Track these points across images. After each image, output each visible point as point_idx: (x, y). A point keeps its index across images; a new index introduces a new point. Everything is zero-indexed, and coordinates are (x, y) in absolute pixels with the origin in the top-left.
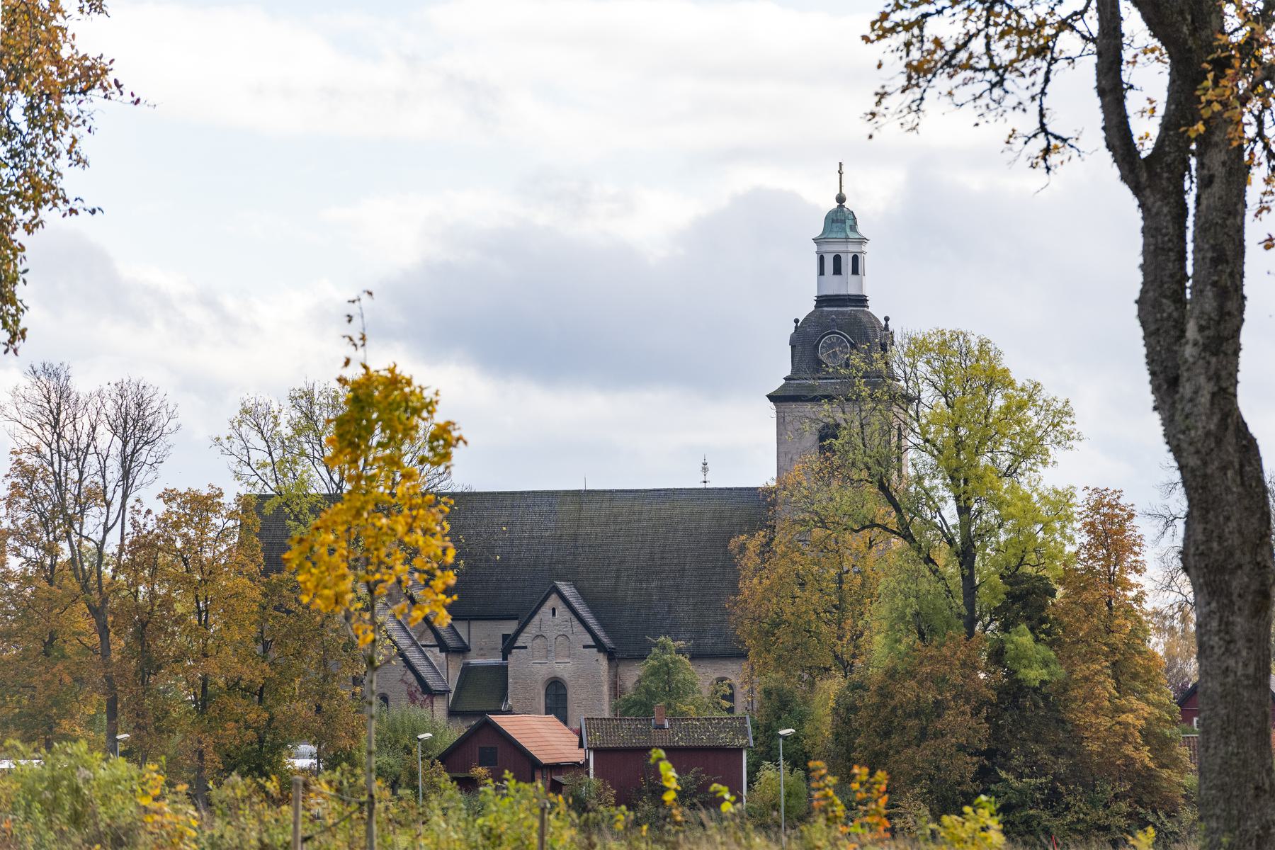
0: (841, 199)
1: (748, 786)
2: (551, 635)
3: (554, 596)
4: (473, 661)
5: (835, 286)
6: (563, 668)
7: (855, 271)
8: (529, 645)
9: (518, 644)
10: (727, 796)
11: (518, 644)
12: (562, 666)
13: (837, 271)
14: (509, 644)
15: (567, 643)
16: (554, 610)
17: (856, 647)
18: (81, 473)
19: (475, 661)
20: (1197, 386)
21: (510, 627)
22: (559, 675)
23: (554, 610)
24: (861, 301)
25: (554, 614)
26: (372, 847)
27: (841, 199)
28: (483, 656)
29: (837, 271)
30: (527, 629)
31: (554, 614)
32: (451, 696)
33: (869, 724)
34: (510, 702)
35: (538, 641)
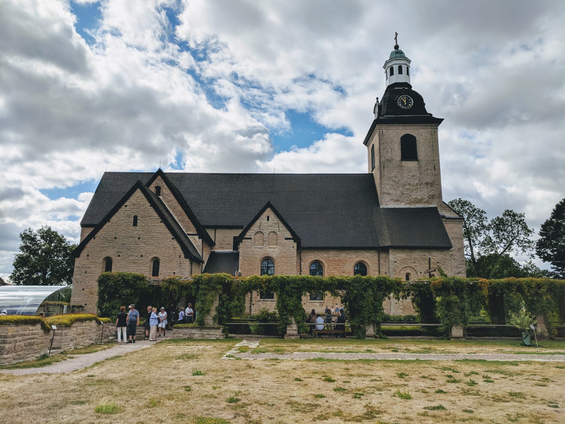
0: (397, 47)
1: (426, 326)
2: (266, 232)
3: (269, 209)
4: (216, 251)
5: (397, 78)
6: (273, 251)
7: (400, 72)
8: (253, 237)
9: (246, 236)
10: (261, 347)
11: (246, 236)
12: (272, 250)
13: (392, 73)
14: (237, 241)
16: (268, 217)
17: (131, 379)
19: (217, 250)
21: (237, 233)
23: (268, 217)
25: (268, 220)
26: (2, 367)
27: (397, 47)
28: (222, 248)
29: (392, 73)
30: (252, 228)
31: (268, 220)
32: (204, 266)
33: (427, 290)
34: (240, 271)
35: (258, 235)
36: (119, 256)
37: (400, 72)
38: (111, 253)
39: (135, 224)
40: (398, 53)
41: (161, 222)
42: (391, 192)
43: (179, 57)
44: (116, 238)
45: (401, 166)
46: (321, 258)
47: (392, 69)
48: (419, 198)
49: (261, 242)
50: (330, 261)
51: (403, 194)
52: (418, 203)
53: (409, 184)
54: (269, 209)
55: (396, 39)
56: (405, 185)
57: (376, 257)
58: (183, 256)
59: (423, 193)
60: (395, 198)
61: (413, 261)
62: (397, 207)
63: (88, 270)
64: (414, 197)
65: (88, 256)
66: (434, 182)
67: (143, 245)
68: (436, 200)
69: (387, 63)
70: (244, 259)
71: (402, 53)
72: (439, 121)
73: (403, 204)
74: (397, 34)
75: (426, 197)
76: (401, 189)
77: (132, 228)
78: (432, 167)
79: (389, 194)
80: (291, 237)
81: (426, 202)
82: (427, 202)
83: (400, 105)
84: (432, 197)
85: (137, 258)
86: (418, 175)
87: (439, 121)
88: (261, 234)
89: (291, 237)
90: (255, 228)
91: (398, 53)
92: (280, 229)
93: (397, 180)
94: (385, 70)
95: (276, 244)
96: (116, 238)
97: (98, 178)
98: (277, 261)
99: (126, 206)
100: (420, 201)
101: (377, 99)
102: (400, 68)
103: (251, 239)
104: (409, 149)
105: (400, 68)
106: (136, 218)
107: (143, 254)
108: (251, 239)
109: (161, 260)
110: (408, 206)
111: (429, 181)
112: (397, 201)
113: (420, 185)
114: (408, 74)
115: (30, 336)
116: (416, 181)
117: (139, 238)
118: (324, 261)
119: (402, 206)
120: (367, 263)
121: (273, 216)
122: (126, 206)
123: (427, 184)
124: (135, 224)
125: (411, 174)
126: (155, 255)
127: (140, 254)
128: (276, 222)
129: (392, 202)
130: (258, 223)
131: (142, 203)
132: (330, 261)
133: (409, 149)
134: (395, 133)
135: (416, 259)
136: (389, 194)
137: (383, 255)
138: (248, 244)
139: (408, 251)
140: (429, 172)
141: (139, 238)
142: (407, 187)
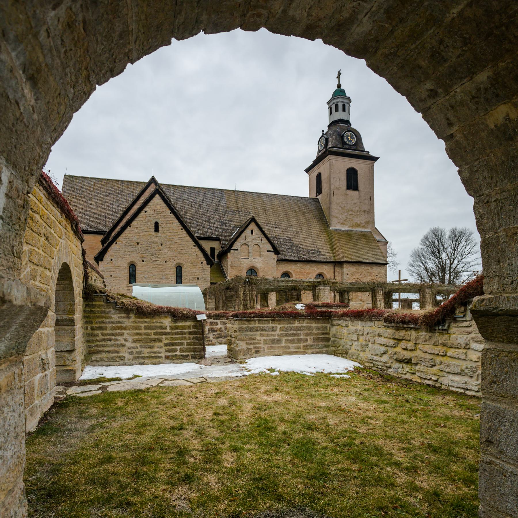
0: (339, 86)
3: (253, 224)
5: (340, 115)
6: (258, 262)
7: (344, 110)
11: (233, 248)
12: (256, 260)
13: (337, 110)
15: (258, 249)
16: (252, 231)
18: (253, 317)
20: (66, 323)
22: (255, 265)
23: (252, 231)
24: (347, 122)
25: (252, 233)
27: (339, 86)
29: (337, 110)
30: (238, 240)
31: (252, 233)
35: (244, 247)
36: (143, 261)
37: (344, 110)
38: (135, 258)
39: (157, 230)
40: (340, 92)
41: (182, 229)
42: (338, 215)
44: (138, 243)
45: (346, 195)
46: (291, 269)
47: (337, 106)
48: (359, 223)
49: (247, 253)
50: (297, 272)
51: (347, 218)
52: (357, 227)
53: (352, 210)
54: (253, 224)
55: (338, 77)
56: (349, 211)
57: (332, 270)
58: (205, 262)
59: (361, 219)
60: (341, 221)
61: (360, 274)
62: (343, 229)
63: (112, 274)
64: (355, 221)
65: (112, 260)
66: (369, 210)
67: (166, 251)
68: (370, 226)
70: (232, 268)
72: (375, 159)
73: (347, 227)
74: (340, 74)
75: (363, 222)
76: (346, 214)
77: (154, 233)
78: (369, 197)
79: (337, 217)
80: (272, 250)
81: (363, 227)
82: (364, 227)
83: (346, 140)
84: (368, 223)
85: (161, 263)
86: (358, 203)
87: (375, 159)
88: (247, 246)
89: (272, 250)
90: (241, 240)
91: (340, 92)
92: (263, 242)
93: (343, 206)
94: (328, 106)
95: (260, 256)
96: (138, 243)
98: (260, 270)
99: (146, 212)
100: (359, 226)
101: (323, 131)
103: (237, 250)
104: (352, 180)
106: (157, 224)
107: (167, 260)
108: (237, 250)
109: (185, 266)
110: (350, 229)
111: (366, 209)
112: (343, 224)
113: (360, 212)
116: (357, 208)
117: (162, 244)
118: (292, 272)
119: (346, 228)
120: (325, 275)
121: (256, 230)
122: (146, 212)
123: (364, 211)
124: (157, 230)
125: (353, 202)
126: (179, 261)
127: (164, 260)
128: (259, 236)
129: (339, 224)
130: (243, 235)
131: (162, 210)
132: (297, 272)
133: (352, 180)
134: (342, 164)
135: (362, 272)
136: (337, 217)
137: (337, 269)
138: (235, 254)
139: (356, 265)
140: (366, 201)
141: (162, 244)
142: (350, 213)
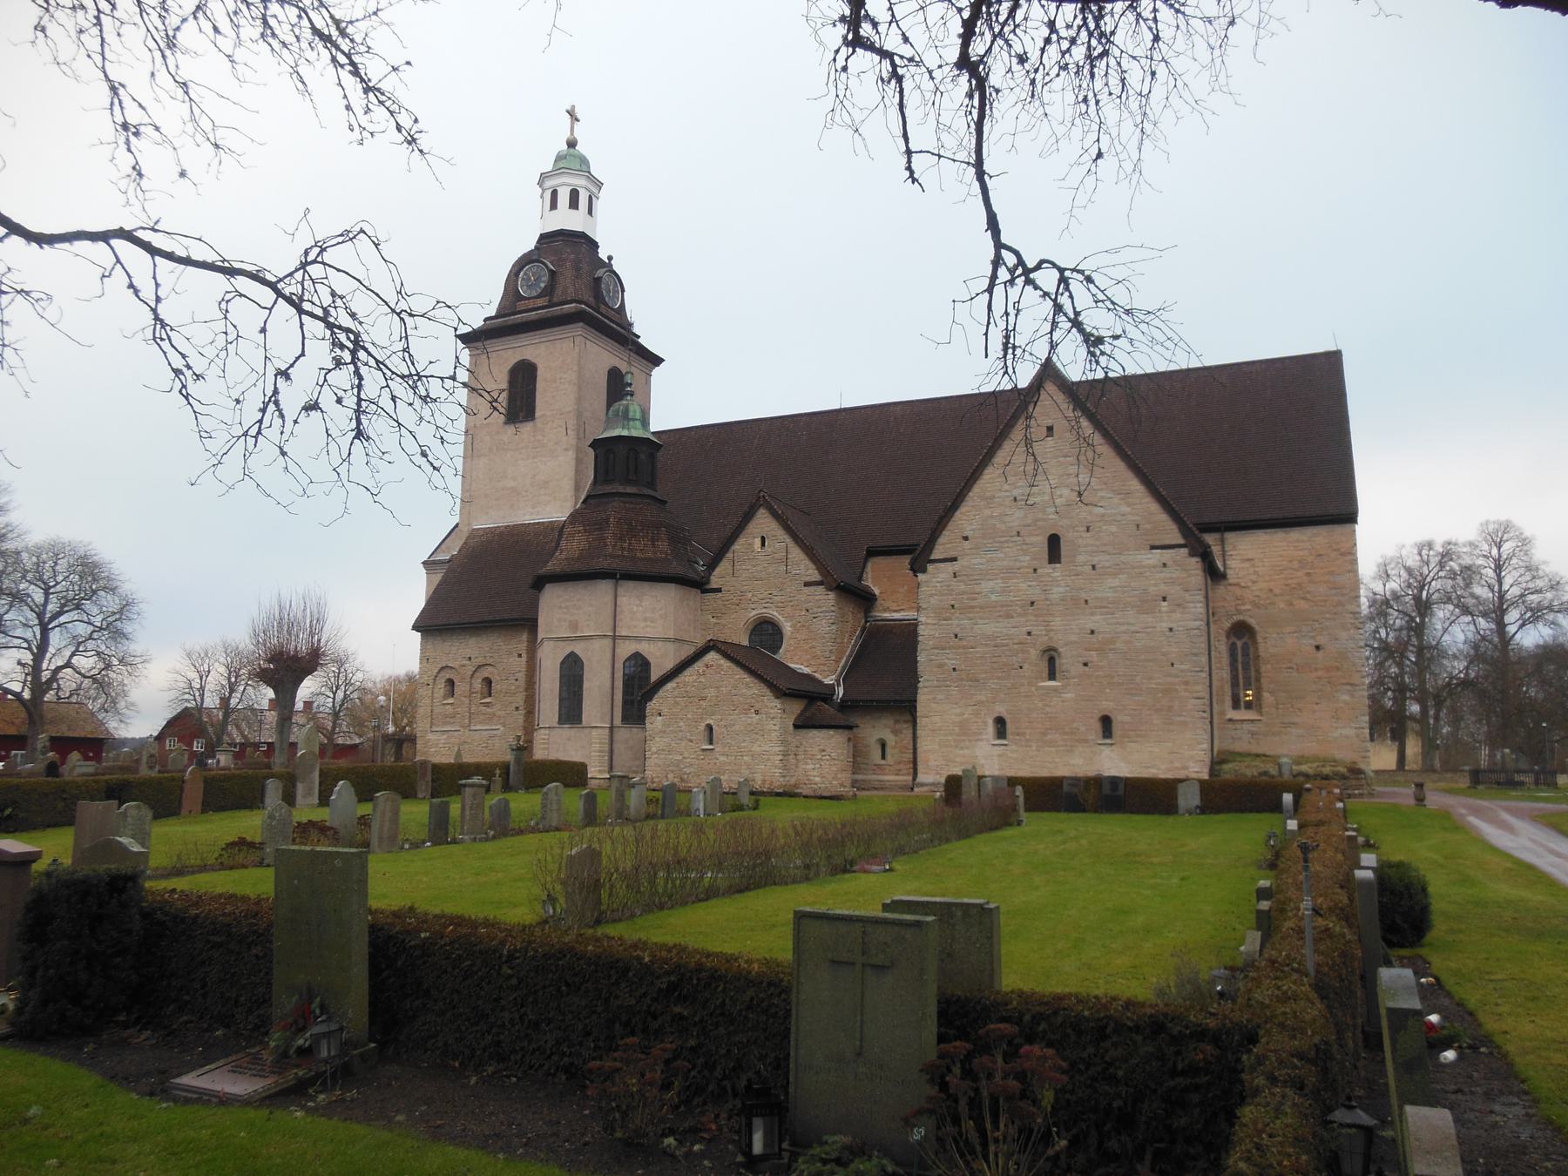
0: (572, 144)
7: (574, 204)
13: (554, 206)
27: (572, 144)
29: (554, 206)
37: (574, 204)
40: (571, 159)
43: (200, 55)
47: (554, 194)
69: (543, 177)
71: (584, 161)
72: (656, 361)
80: (1182, 541)
89: (1182, 541)
91: (571, 159)
97: (943, 780)
102: (574, 195)
105: (574, 195)
114: (590, 212)
115: (1240, 658)
